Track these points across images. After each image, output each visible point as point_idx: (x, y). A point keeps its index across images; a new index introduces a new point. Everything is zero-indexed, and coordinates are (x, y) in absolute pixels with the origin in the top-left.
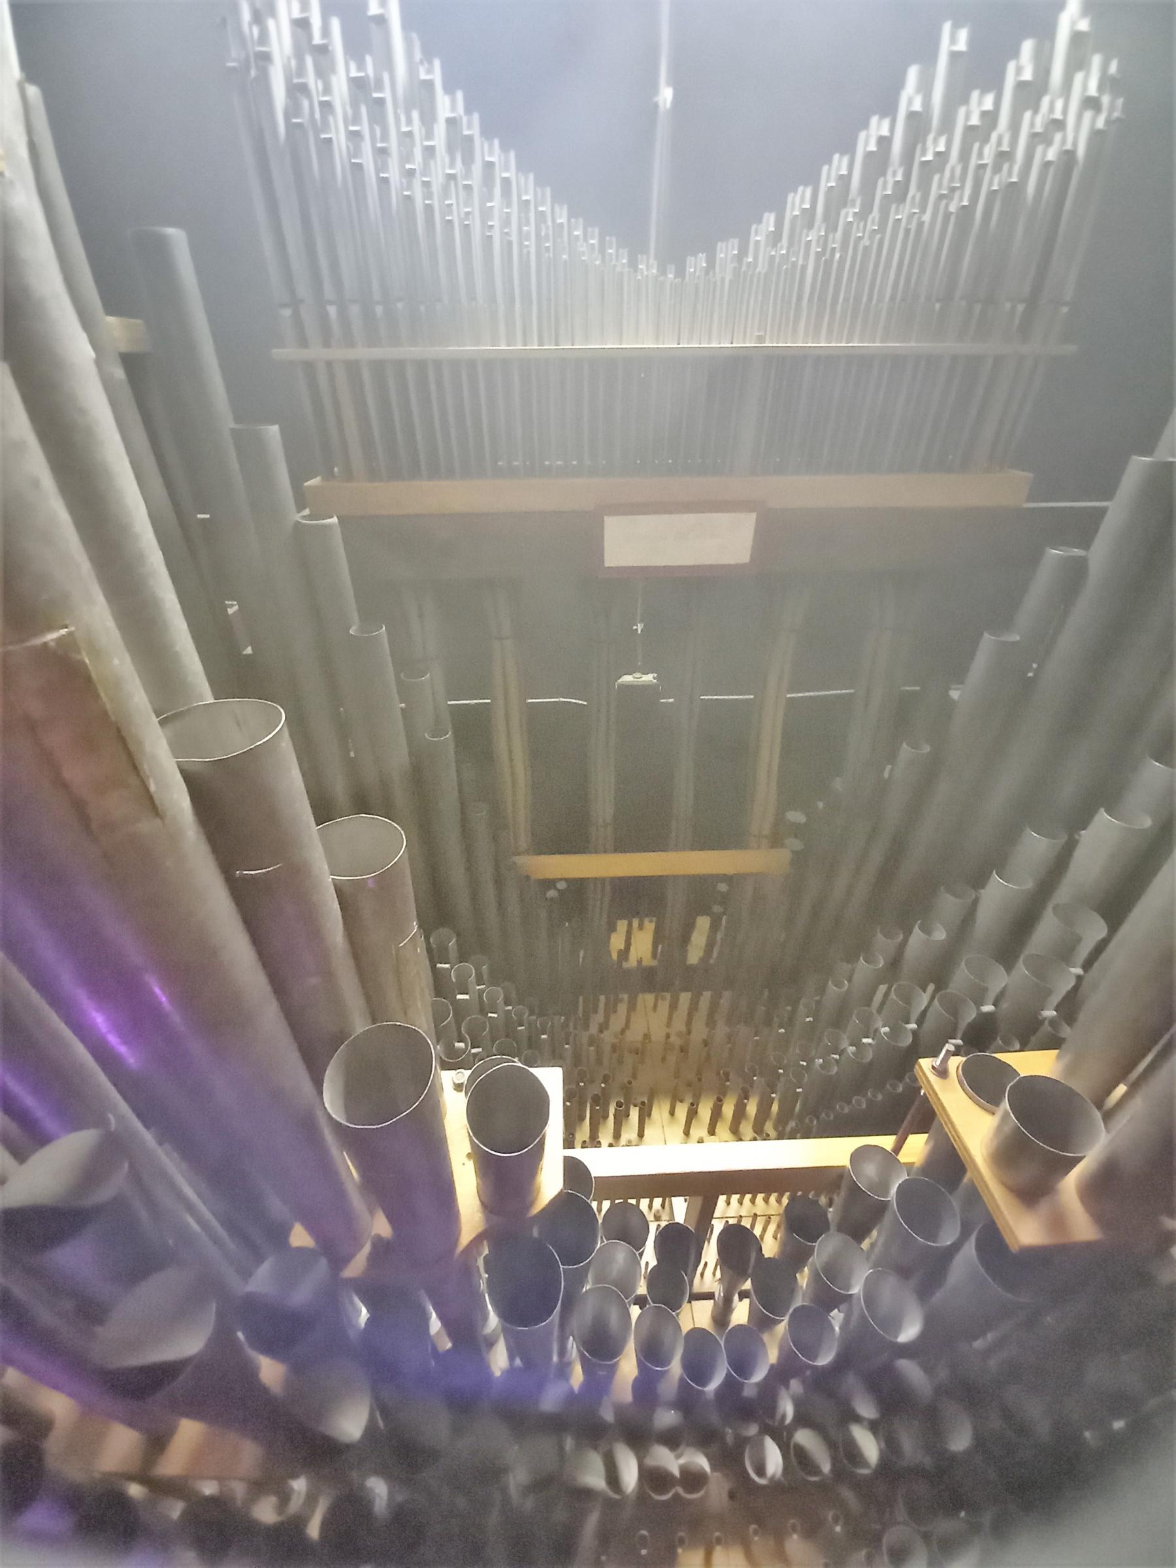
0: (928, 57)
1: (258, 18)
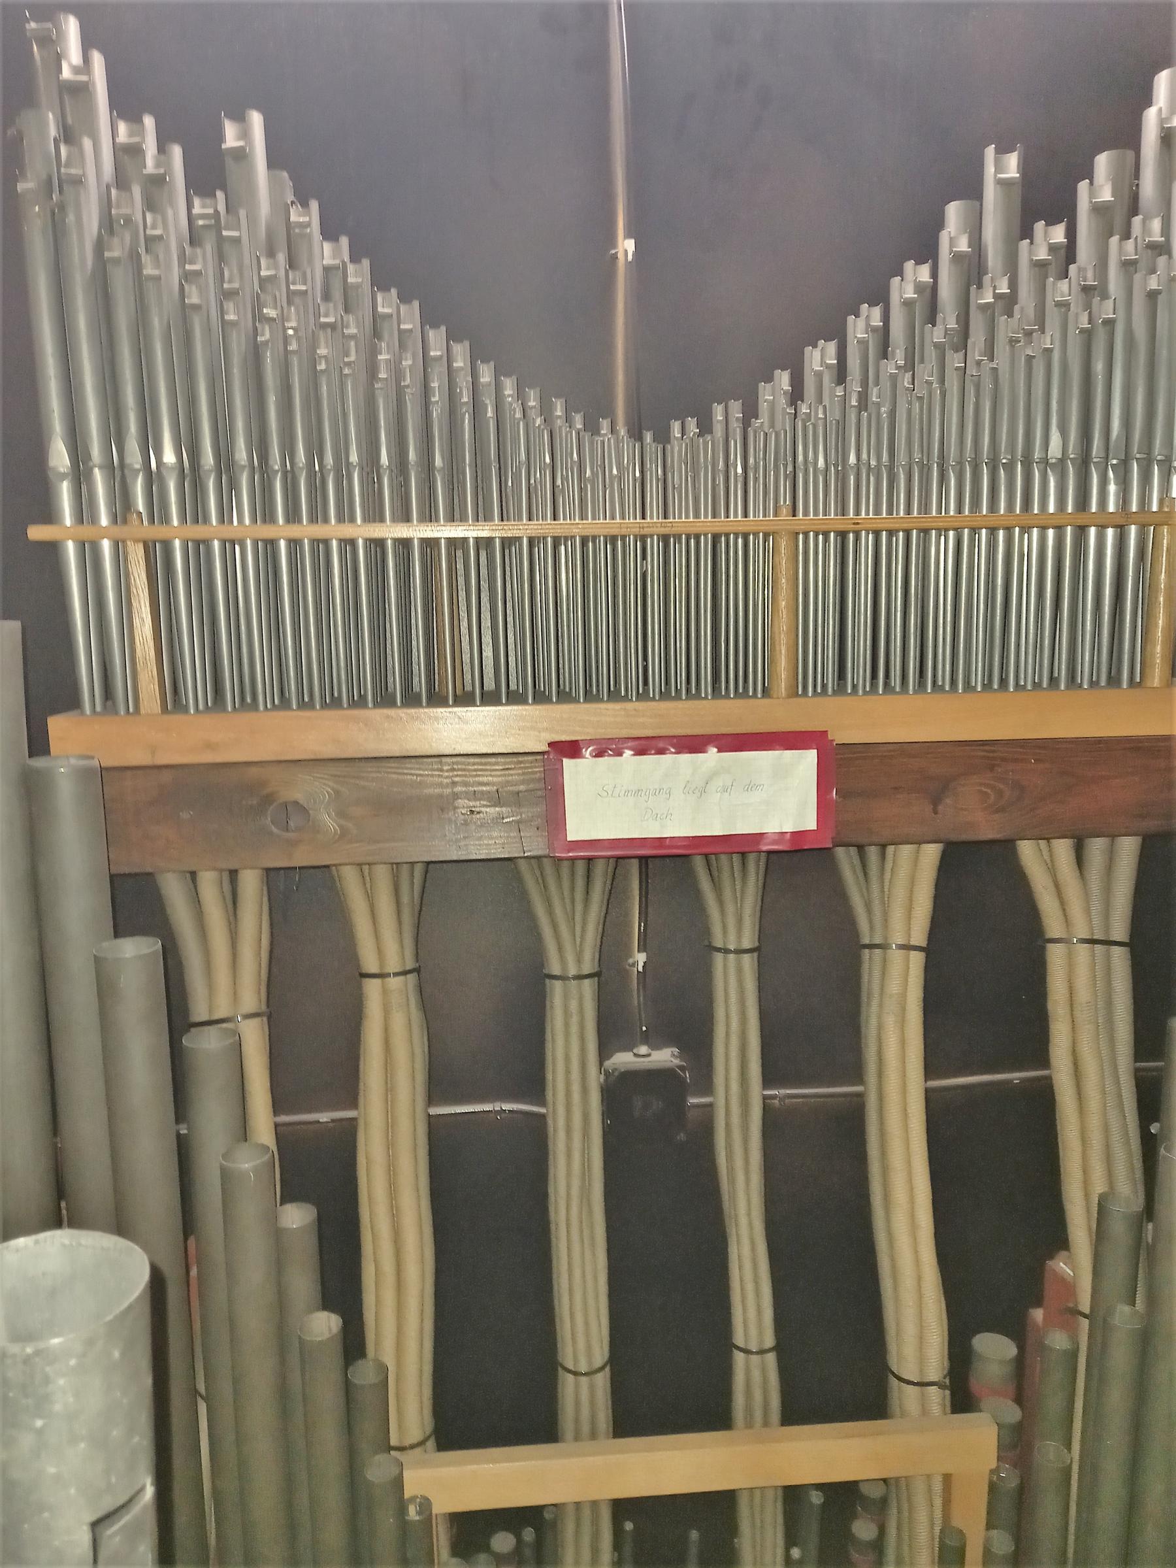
0: (972, 191)
1: (68, 136)
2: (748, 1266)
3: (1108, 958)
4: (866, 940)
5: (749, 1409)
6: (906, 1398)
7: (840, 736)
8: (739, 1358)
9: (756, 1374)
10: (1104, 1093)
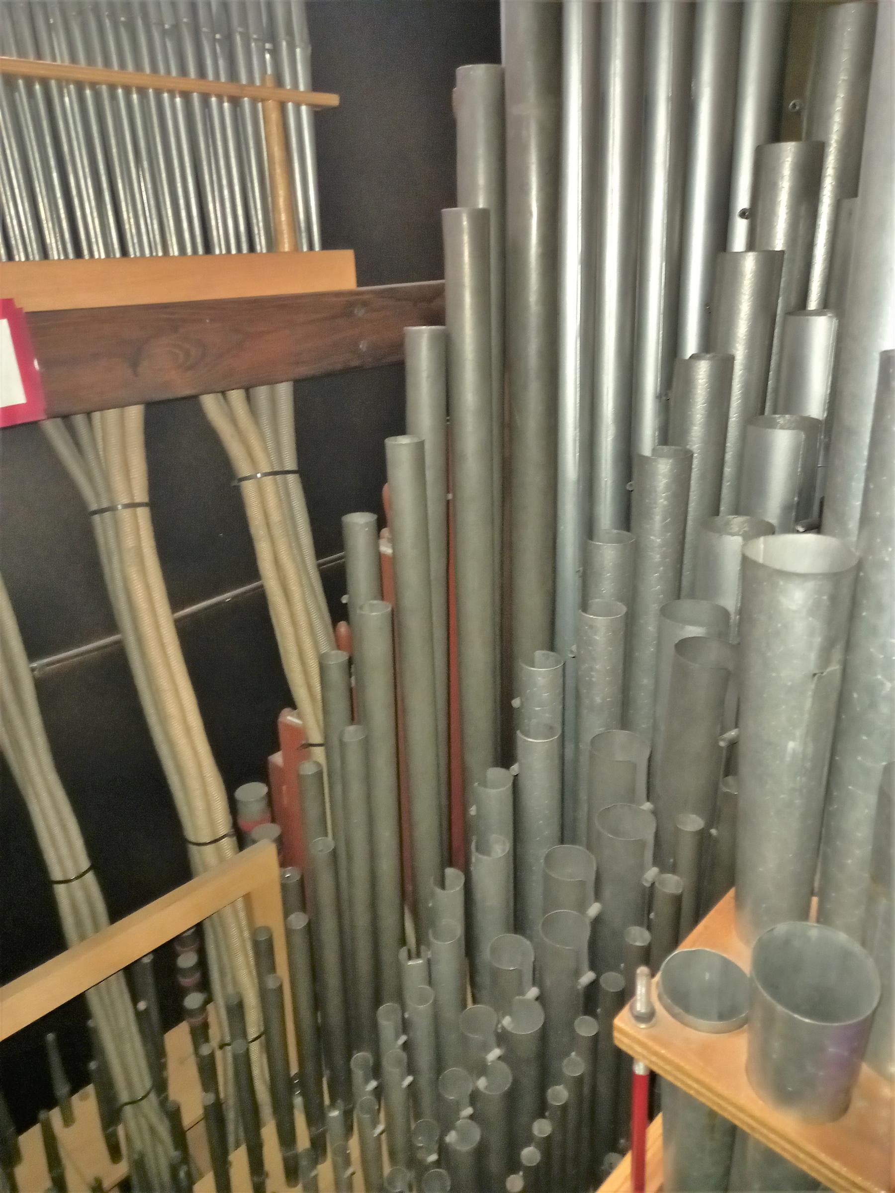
2: (51, 813)
3: (286, 484)
4: (94, 507)
5: (79, 923)
6: (204, 857)
7: (30, 304)
8: (61, 891)
9: (79, 895)
10: (302, 586)
